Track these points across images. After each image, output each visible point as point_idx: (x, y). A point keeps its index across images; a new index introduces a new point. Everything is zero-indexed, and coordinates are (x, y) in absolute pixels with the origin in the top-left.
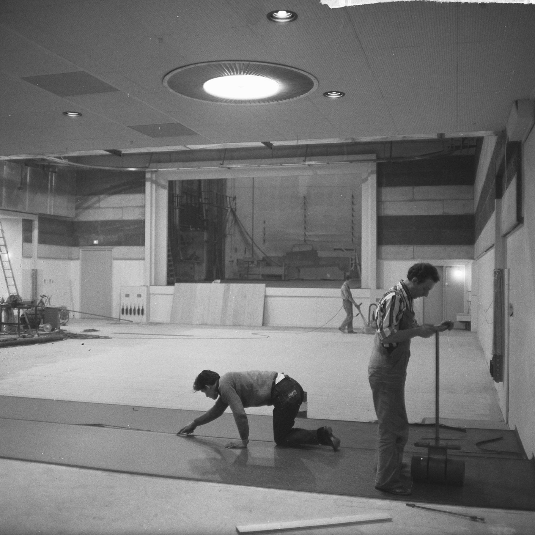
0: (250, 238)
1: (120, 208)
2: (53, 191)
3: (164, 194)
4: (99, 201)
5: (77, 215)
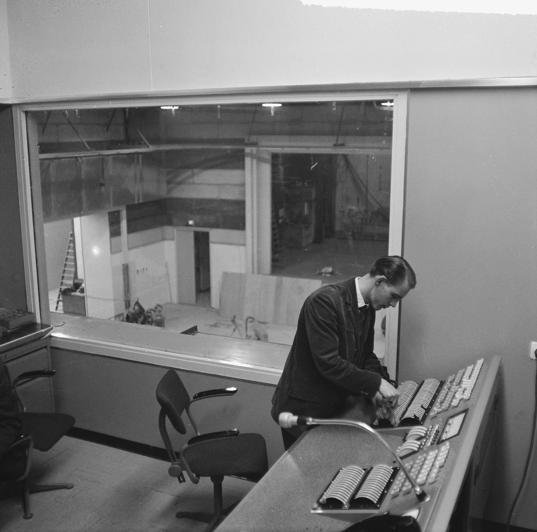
0: (364, 186)
3: (267, 169)
4: (193, 175)
5: (169, 191)
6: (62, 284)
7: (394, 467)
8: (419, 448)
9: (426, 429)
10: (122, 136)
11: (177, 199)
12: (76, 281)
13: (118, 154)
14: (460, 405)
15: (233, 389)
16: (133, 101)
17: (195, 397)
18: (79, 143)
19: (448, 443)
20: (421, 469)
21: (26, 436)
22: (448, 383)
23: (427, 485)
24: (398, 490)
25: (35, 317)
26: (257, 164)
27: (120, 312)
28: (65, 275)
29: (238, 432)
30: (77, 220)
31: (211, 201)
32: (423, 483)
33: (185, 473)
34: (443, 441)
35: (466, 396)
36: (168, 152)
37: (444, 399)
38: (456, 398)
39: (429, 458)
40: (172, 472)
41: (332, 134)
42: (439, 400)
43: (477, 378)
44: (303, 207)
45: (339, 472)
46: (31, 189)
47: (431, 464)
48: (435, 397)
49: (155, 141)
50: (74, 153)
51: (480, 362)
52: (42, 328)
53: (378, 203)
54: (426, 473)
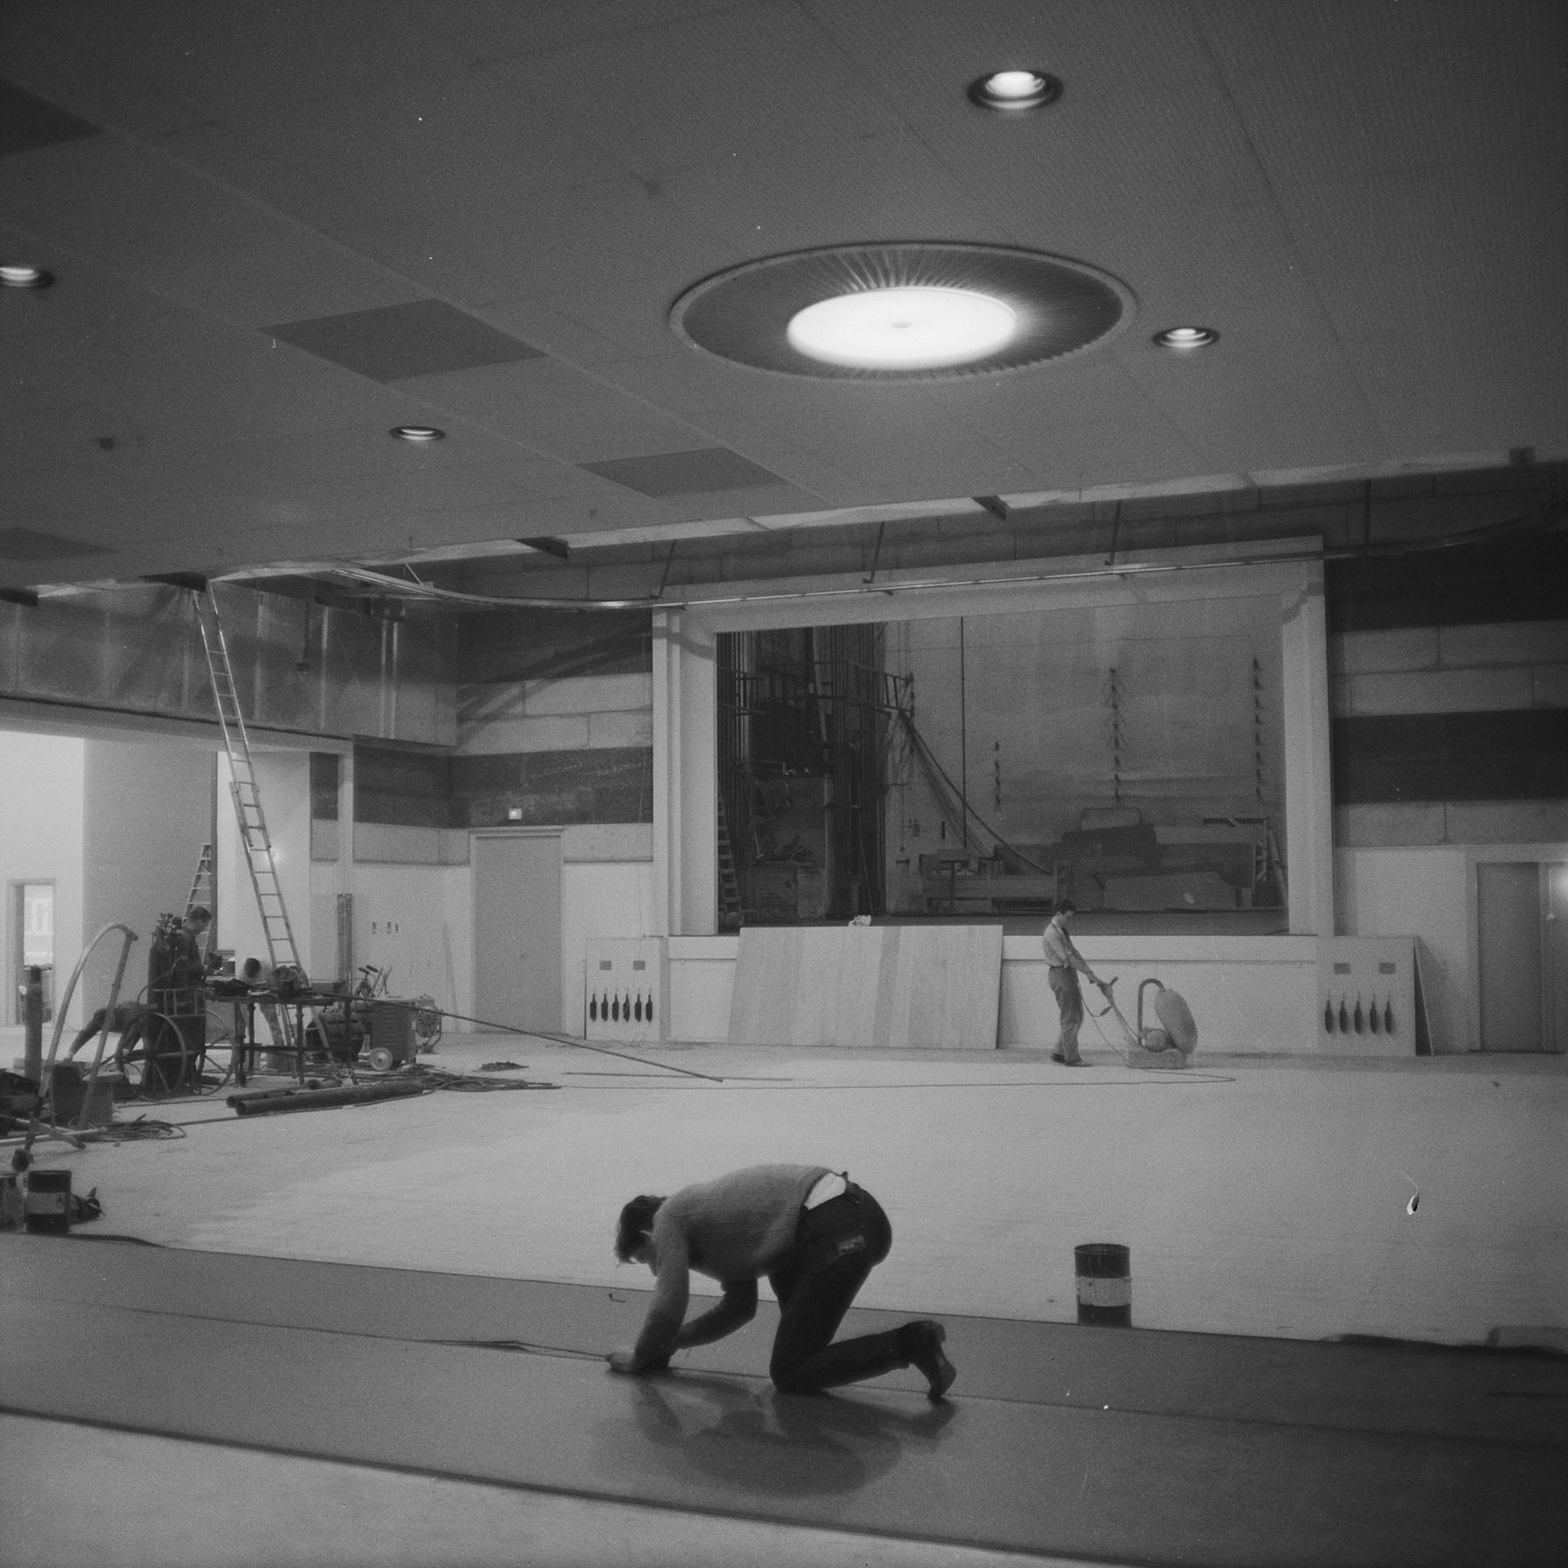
3: (706, 671)
4: (523, 697)
5: (462, 739)
31: (566, 755)
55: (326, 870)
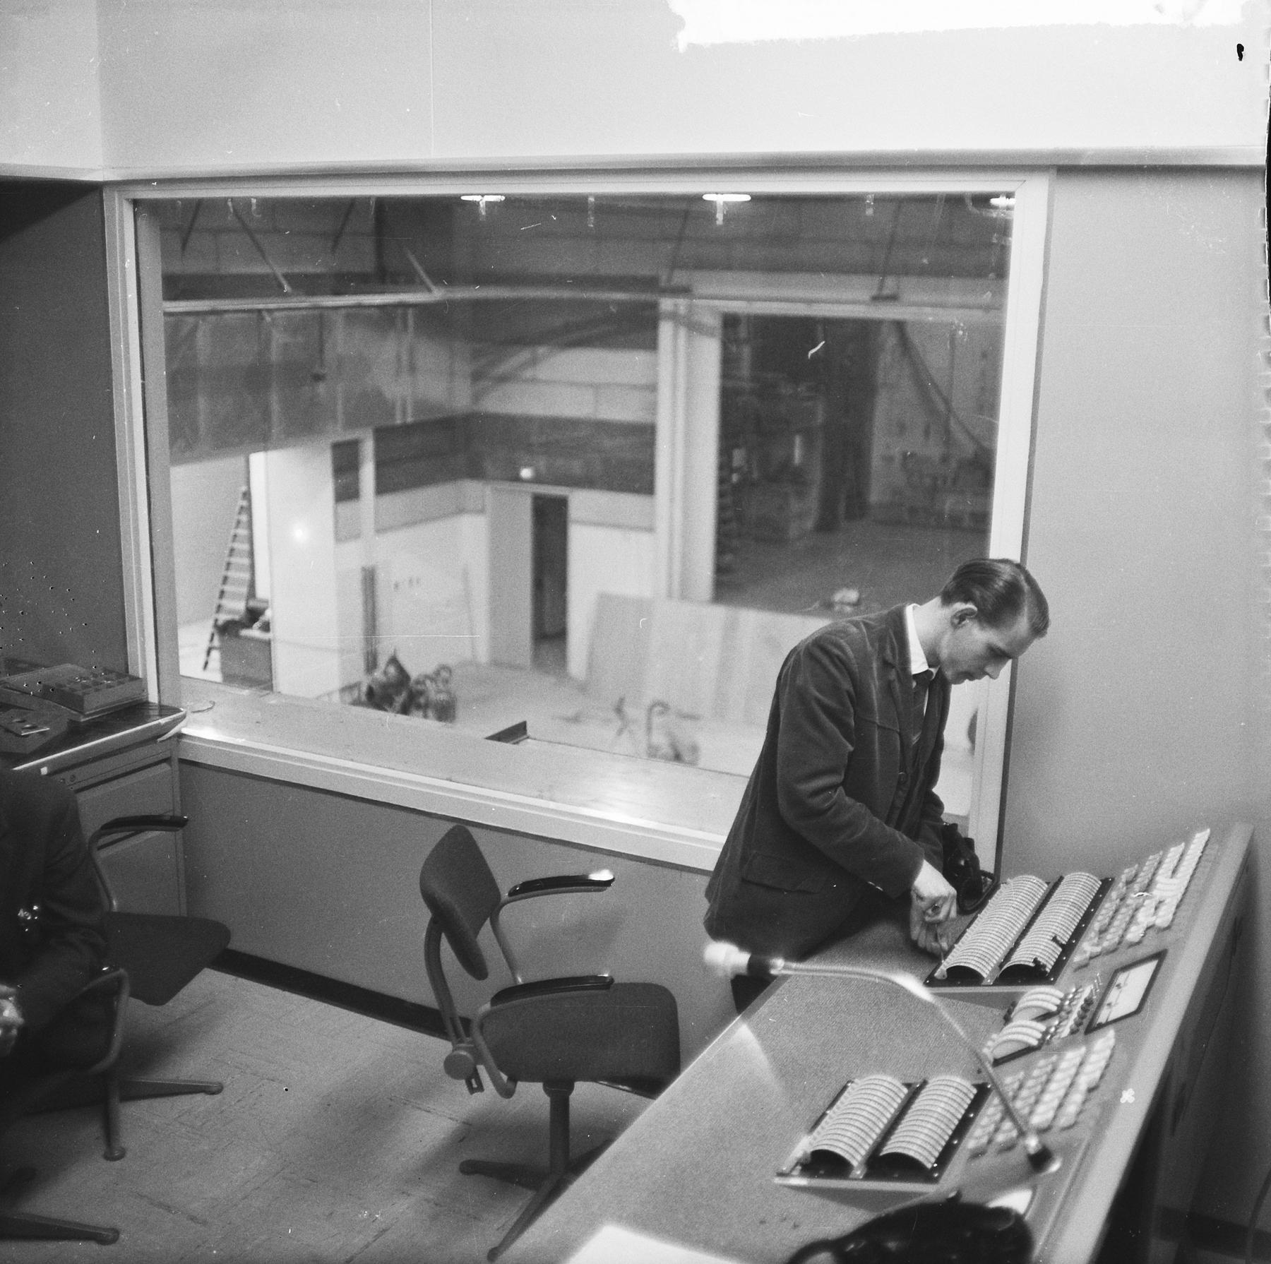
1: (591, 385)
2: (399, 404)
3: (710, 351)
4: (534, 362)
5: (477, 397)
6: (219, 608)
7: (981, 1082)
8: (1043, 1042)
9: (1062, 995)
10: (367, 264)
11: (496, 418)
12: (252, 604)
13: (359, 306)
14: (1145, 942)
15: (604, 875)
16: (377, 182)
17: (513, 893)
18: (267, 276)
19: (1111, 1033)
20: (1043, 1091)
21: (113, 968)
22: (1121, 885)
23: (1055, 1130)
24: (985, 1140)
25: (144, 689)
26: (689, 339)
27: (353, 681)
28: (227, 588)
29: (612, 980)
30: (258, 460)
31: (574, 423)
32: (1046, 1125)
33: (482, 1070)
34: (1101, 1026)
35: (1163, 918)
36: (477, 304)
37: (1110, 924)
38: (1138, 924)
39: (1063, 1065)
40: (453, 1067)
41: (869, 270)
42: (1096, 925)
43: (1192, 876)
44: (792, 446)
45: (845, 1088)
46: (143, 385)
47: (1068, 1082)
48: (1087, 917)
49: (444, 276)
50: (255, 300)
51: (1200, 838)
52: (161, 716)
53: (972, 438)
54: (1056, 1103)
55: (352, 547)
